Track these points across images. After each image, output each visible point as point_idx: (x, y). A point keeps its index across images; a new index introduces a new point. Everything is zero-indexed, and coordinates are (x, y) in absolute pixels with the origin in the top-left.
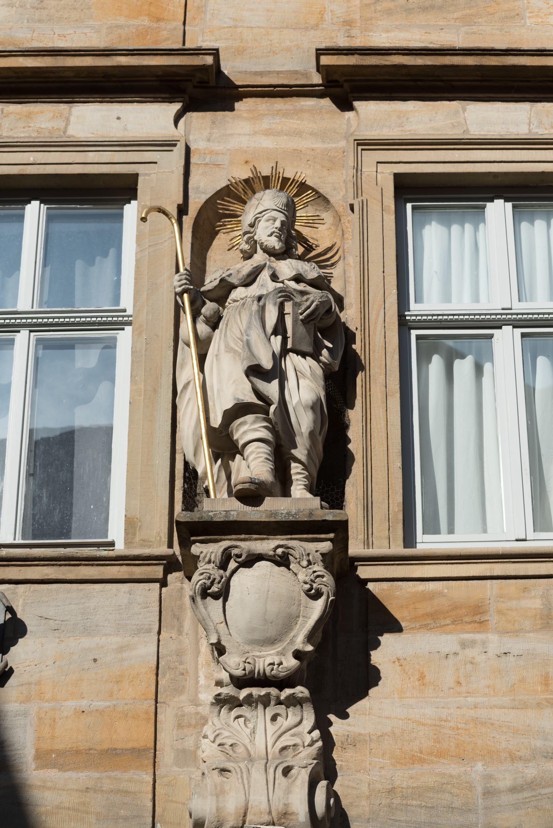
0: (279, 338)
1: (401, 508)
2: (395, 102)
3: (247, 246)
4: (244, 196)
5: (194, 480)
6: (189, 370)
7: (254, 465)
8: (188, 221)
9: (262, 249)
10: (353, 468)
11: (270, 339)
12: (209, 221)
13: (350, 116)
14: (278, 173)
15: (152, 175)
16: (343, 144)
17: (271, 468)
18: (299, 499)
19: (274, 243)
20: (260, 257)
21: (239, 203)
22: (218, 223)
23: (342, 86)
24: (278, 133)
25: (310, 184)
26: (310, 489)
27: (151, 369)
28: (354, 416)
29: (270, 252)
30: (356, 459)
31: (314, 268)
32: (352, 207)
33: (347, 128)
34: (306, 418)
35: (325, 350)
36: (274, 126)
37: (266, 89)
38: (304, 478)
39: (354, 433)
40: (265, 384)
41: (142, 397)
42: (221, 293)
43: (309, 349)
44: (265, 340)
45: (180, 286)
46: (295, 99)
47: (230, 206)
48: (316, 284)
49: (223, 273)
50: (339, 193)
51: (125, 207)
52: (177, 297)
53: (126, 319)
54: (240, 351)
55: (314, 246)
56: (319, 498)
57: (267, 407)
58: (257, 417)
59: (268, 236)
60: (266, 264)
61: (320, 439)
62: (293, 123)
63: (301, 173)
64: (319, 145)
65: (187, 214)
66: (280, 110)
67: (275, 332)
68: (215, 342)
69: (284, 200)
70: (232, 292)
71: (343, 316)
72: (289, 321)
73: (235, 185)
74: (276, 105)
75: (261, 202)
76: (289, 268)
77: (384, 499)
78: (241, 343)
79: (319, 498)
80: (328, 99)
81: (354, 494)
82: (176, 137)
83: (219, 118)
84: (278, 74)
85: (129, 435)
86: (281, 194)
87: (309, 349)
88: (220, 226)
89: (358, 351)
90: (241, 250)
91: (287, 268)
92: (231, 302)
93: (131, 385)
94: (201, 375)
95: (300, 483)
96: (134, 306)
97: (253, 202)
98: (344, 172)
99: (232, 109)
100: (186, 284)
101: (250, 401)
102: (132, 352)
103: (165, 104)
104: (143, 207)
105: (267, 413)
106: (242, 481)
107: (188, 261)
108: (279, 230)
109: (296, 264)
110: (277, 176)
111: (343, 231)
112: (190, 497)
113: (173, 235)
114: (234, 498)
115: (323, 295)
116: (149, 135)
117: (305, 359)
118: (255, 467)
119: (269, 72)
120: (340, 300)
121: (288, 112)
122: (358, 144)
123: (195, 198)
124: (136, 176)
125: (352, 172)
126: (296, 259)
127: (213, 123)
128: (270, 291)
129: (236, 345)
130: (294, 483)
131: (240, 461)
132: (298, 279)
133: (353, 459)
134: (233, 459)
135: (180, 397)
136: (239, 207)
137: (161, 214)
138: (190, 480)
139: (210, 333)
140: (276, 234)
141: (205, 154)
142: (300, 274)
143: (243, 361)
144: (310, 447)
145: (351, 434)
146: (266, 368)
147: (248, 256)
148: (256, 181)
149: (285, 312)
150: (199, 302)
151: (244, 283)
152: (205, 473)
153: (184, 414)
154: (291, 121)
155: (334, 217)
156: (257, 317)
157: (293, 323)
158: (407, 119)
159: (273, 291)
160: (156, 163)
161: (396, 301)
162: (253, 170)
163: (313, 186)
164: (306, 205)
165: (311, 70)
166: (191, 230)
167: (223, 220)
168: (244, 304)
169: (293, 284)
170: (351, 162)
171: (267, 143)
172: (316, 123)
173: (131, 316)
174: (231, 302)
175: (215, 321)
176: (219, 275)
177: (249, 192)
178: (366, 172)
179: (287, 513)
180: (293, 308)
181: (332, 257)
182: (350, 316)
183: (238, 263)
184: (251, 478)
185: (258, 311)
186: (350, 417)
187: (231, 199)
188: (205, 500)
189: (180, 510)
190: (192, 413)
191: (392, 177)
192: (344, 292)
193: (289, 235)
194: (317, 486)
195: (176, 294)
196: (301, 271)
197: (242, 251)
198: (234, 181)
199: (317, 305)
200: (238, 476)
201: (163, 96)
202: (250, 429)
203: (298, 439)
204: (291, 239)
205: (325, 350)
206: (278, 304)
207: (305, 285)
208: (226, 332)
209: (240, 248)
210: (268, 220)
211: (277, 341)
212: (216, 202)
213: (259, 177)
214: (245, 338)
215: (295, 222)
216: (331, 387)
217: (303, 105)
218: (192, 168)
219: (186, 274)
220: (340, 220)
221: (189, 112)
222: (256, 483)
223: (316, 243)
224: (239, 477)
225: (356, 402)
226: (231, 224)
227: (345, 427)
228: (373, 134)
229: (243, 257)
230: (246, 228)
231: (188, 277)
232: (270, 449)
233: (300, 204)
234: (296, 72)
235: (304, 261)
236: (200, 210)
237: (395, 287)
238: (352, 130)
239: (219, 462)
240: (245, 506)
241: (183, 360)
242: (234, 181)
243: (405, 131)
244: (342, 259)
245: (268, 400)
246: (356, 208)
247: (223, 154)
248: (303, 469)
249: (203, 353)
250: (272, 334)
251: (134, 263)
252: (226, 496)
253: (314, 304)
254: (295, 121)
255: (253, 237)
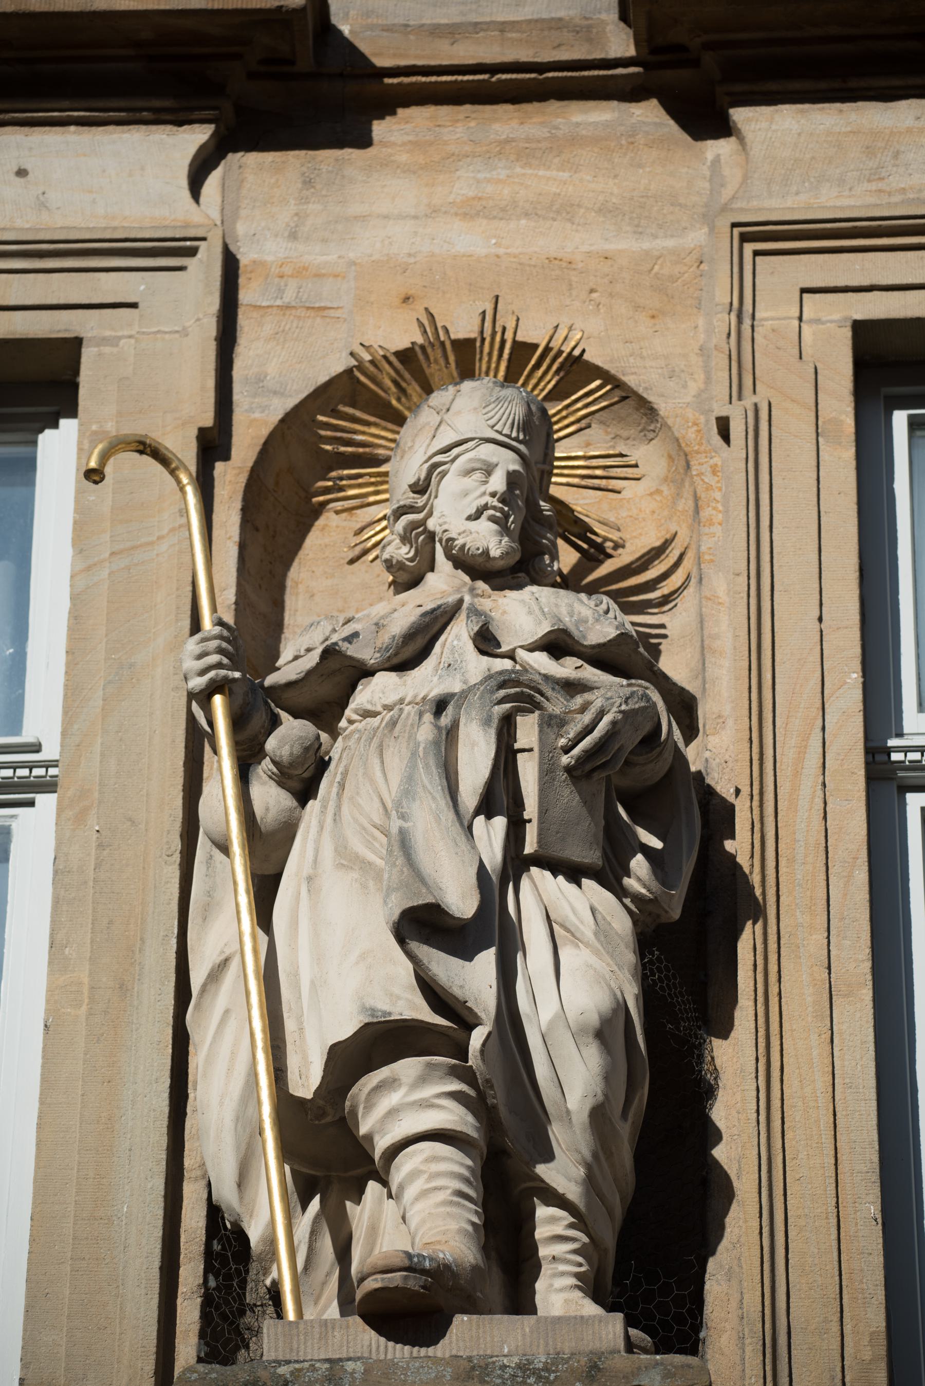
0: (500, 823)
1: (883, 1351)
2: (860, 104)
3: (405, 549)
4: (399, 400)
5: (236, 1263)
6: (225, 927)
7: (421, 1212)
8: (229, 477)
9: (449, 556)
10: (728, 1220)
11: (470, 828)
12: (291, 480)
13: (721, 152)
14: (499, 329)
15: (122, 342)
16: (697, 237)
17: (473, 1224)
18: (559, 1319)
19: (487, 538)
20: (443, 583)
21: (383, 423)
22: (321, 484)
23: (695, 63)
24: (503, 210)
25: (598, 362)
26: (595, 1287)
27: (111, 922)
28: (731, 1057)
29: (475, 567)
30: (737, 1192)
31: (607, 612)
32: (724, 428)
33: (711, 191)
34: (581, 1067)
35: (639, 857)
36: (490, 189)
37: (466, 78)
38: (575, 1252)
39: (732, 1111)
40: (455, 963)
41: (84, 1008)
42: (325, 690)
43: (592, 856)
44: (456, 831)
45: (202, 673)
46: (553, 106)
47: (355, 432)
48: (606, 658)
49: (334, 631)
50: (685, 386)
51: (41, 437)
52: (194, 705)
53: (38, 772)
54: (380, 863)
55: (609, 544)
56: (620, 1316)
57: (460, 1035)
58: (429, 1065)
59: (469, 518)
60: (461, 601)
61: (625, 1131)
62: (547, 180)
63: (570, 329)
64: (626, 244)
65: (226, 457)
66: (508, 141)
67: (487, 808)
68: (305, 839)
69: (518, 411)
70: (360, 687)
71: (695, 756)
72: (528, 771)
73: (372, 368)
74: (496, 126)
75: (446, 417)
76: (530, 613)
77: (826, 1320)
78: (384, 840)
79: (620, 1316)
80: (654, 102)
81: (734, 1304)
82: (197, 226)
83: (324, 168)
84: (502, 31)
85: (39, 1126)
86: (509, 392)
87: (592, 856)
88: (327, 490)
89: (743, 860)
90: (386, 561)
91: (522, 614)
92: (355, 717)
93: (51, 972)
94: (263, 938)
95: (562, 1268)
96: (64, 734)
97: (426, 417)
98: (701, 322)
99: (364, 141)
100: (219, 666)
101: (408, 1015)
102: (56, 872)
103: (162, 127)
104: (95, 437)
105: (462, 1054)
106: (381, 1263)
107: (228, 596)
108: (503, 501)
109: (553, 600)
110: (498, 338)
111: (696, 499)
112: (224, 1317)
113: (183, 520)
114: (358, 1319)
115: (633, 693)
116: (115, 223)
117: (579, 885)
118: (423, 1221)
119: (477, 27)
120: (684, 707)
121: (534, 145)
122: (745, 238)
123: (251, 410)
124: (76, 344)
125: (723, 321)
126: (554, 585)
127: (308, 183)
128: (473, 680)
129: (369, 845)
130: (546, 1269)
131: (380, 1202)
132: (557, 644)
133: (727, 1193)
134: (358, 1195)
135: (198, 1005)
136: (383, 433)
137: (147, 460)
138: (224, 1262)
139: (291, 810)
140: (491, 512)
141: (282, 277)
142: (565, 632)
143: (387, 896)
144: (595, 1155)
145: (723, 1114)
146: (458, 914)
147: (407, 579)
148: (435, 354)
149: (517, 746)
150: (258, 720)
151: (395, 661)
152: (271, 1242)
153: (209, 1060)
154: (541, 173)
155: (670, 457)
156: (432, 762)
157: (541, 779)
158: (896, 155)
159: (481, 683)
160: (134, 305)
161: (860, 706)
162: (426, 323)
163: (606, 367)
164: (583, 425)
165: (604, 16)
166: (238, 505)
167: (334, 474)
168: (393, 723)
169: (541, 662)
170: (722, 291)
171: (468, 240)
172: (616, 176)
173: (54, 764)
174: (355, 717)
175: (306, 775)
176: (321, 638)
177: (414, 389)
178: (766, 319)
179: (519, 1366)
180: (541, 731)
181: (665, 576)
182: (717, 754)
183: (381, 599)
184: (409, 1256)
185: (436, 743)
186: (718, 1062)
187: (361, 410)
188: (268, 1326)
189: (193, 1360)
190: (233, 1055)
191: (848, 333)
192: (699, 682)
193: (533, 515)
194: (617, 1279)
195: (191, 696)
196: (568, 622)
197: (389, 565)
198: (367, 357)
199: (614, 723)
200: (372, 1250)
201: (157, 103)
202: (407, 1104)
203: (557, 1133)
204: (537, 528)
205: (639, 857)
206: (495, 723)
207: (580, 662)
208: (339, 807)
209: (386, 556)
210: (468, 472)
211: (491, 835)
212: (314, 421)
213: (443, 344)
214: (395, 825)
215: (551, 474)
216: (659, 970)
217: (578, 124)
218: (245, 321)
219: (220, 637)
220: (688, 466)
221: (236, 150)
222: (424, 1272)
223: (614, 536)
224: (376, 1252)
225: (738, 1014)
226: (360, 486)
227: (703, 1092)
228: (789, 203)
229: (393, 583)
230: (402, 495)
231: (224, 645)
232: (469, 1162)
233: (566, 422)
234: (557, 24)
235: (578, 589)
236: (266, 444)
237: (857, 665)
238: (727, 194)
239: (315, 1204)
240: (391, 1344)
241: (209, 894)
242: (367, 357)
243: (890, 194)
244: (693, 581)
245: (464, 1013)
246: (737, 429)
247: (336, 276)
248: (571, 1226)
249: (270, 870)
250: (477, 813)
251: (66, 604)
252: (333, 1312)
253: (607, 719)
254: (554, 173)
255: (423, 522)
